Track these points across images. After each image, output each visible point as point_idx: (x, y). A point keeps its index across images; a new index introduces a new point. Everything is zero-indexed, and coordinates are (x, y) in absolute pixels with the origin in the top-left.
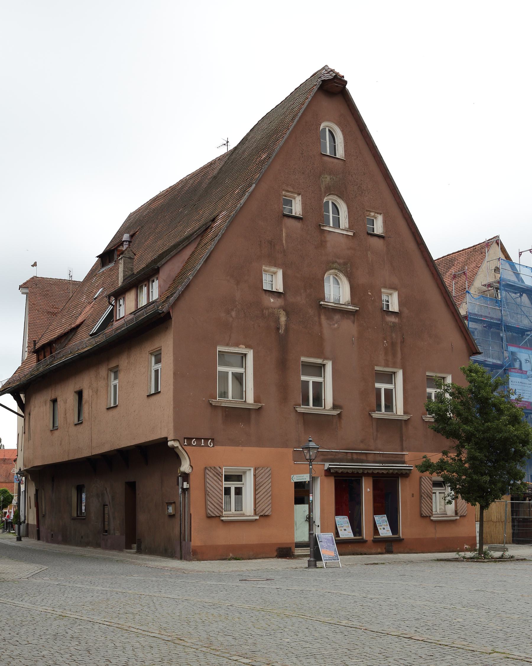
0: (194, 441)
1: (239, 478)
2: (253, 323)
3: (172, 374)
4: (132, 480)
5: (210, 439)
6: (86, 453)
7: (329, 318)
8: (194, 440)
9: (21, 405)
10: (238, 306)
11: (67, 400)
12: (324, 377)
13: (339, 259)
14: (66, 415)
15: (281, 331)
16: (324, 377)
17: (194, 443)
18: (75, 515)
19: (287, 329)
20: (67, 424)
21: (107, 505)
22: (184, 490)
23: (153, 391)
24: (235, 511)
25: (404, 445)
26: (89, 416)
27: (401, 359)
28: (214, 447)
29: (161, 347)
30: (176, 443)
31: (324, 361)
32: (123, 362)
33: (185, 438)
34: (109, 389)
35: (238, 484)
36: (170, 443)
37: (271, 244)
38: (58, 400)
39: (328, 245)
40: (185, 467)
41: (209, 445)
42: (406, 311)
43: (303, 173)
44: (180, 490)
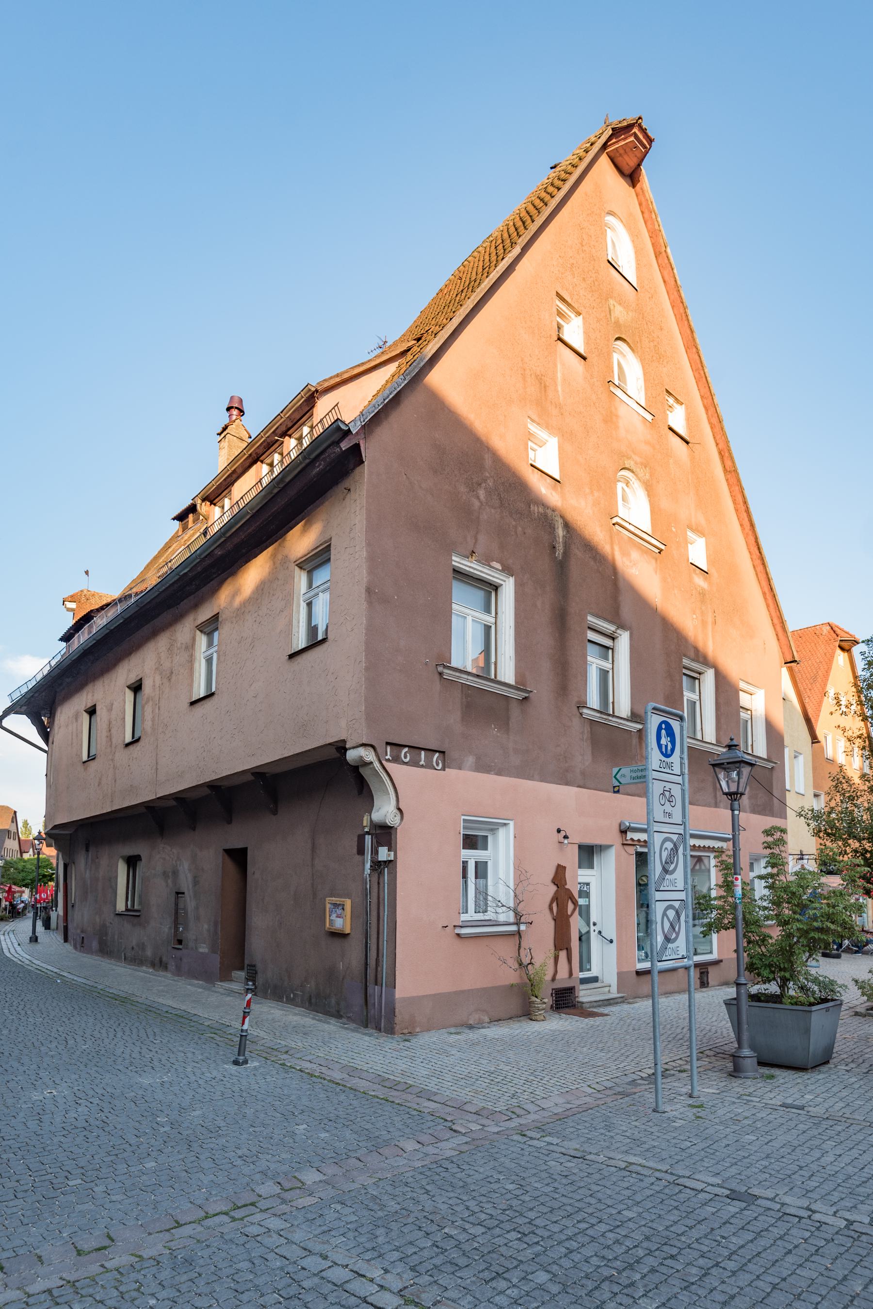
2: (514, 523)
4: (236, 844)
8: (406, 749)
10: (489, 481)
11: (112, 704)
13: (635, 454)
14: (110, 731)
15: (560, 552)
17: (405, 757)
19: (566, 553)
20: (111, 746)
21: (183, 893)
22: (378, 866)
23: (302, 644)
26: (153, 725)
28: (444, 770)
30: (367, 753)
31: (618, 631)
33: (388, 743)
34: (196, 665)
36: (352, 755)
38: (98, 708)
41: (435, 764)
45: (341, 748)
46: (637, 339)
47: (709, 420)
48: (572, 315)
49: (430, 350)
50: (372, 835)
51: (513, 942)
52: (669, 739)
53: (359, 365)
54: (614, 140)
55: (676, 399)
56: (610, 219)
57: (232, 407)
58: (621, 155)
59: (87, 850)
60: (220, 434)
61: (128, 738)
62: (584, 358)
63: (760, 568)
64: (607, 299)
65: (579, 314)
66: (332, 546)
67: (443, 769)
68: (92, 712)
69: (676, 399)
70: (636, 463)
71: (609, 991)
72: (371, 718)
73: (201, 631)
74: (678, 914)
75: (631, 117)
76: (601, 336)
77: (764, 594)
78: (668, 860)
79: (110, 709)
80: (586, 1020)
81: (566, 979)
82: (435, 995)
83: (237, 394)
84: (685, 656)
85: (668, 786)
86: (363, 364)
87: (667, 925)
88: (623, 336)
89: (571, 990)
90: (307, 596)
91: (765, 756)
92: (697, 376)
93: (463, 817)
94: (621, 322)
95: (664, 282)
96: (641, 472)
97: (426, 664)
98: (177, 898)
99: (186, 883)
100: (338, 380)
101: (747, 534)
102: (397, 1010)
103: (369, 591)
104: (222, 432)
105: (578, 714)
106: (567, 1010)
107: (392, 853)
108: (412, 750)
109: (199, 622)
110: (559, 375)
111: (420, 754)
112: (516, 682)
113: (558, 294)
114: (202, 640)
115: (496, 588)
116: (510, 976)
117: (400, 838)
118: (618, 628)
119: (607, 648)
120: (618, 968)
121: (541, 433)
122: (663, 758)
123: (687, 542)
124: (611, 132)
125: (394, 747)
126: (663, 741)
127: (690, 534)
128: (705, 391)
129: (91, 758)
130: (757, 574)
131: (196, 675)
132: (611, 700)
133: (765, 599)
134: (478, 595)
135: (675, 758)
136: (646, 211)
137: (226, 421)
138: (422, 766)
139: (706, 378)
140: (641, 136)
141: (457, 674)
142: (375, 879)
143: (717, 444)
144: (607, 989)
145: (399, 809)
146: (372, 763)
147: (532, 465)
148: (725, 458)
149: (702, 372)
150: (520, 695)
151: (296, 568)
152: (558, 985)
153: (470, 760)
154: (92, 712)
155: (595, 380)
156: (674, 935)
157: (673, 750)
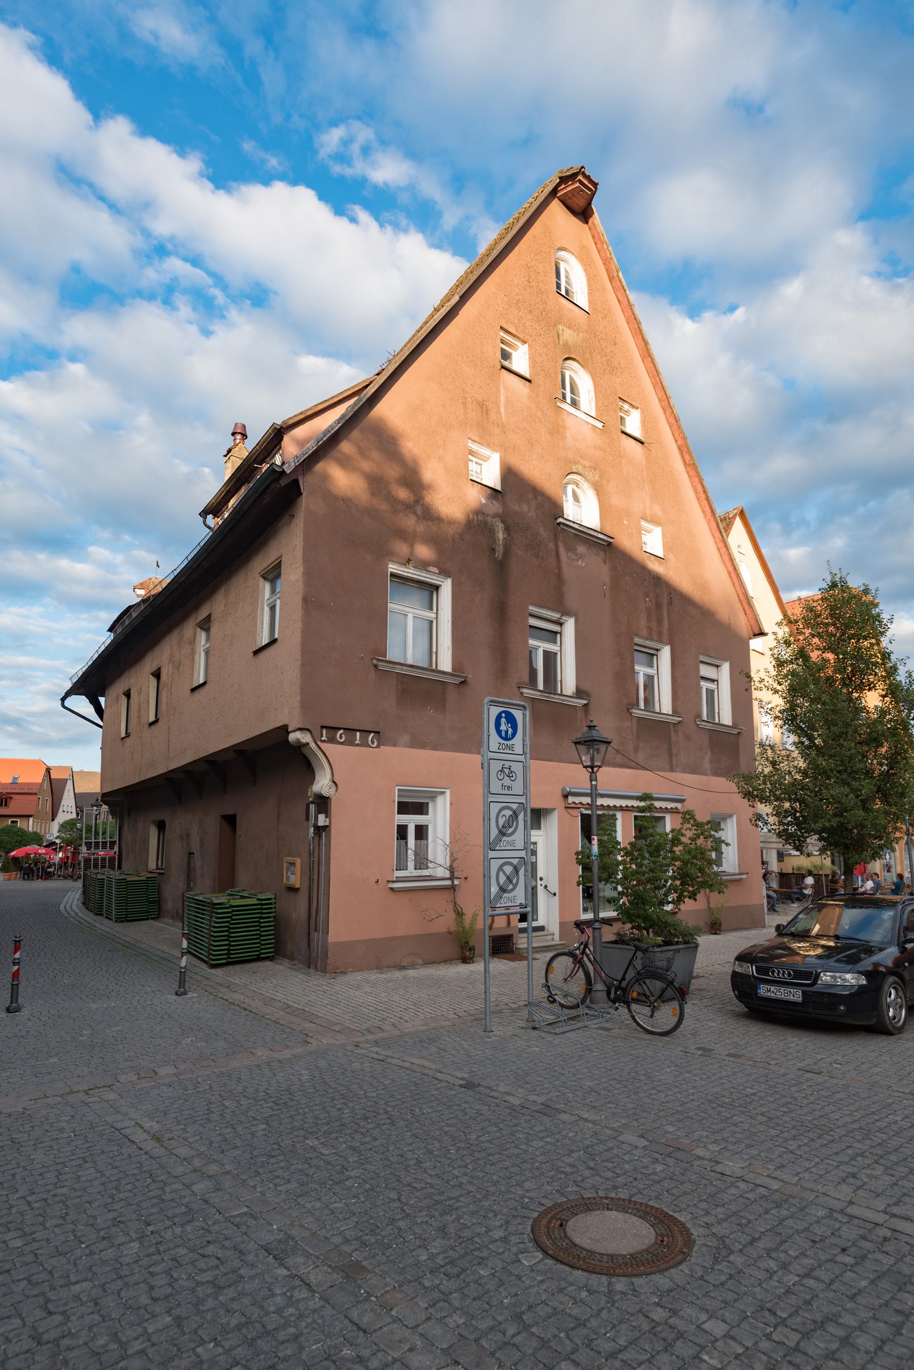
0: (341, 734)
1: (420, 809)
3: (301, 600)
4: (231, 812)
5: (371, 732)
6: (161, 769)
7: (570, 549)
8: (342, 731)
9: (100, 711)
12: (561, 644)
15: (499, 554)
16: (561, 644)
17: (341, 738)
18: (154, 867)
19: (506, 553)
21: (193, 854)
22: (319, 830)
23: (265, 640)
24: (415, 869)
25: (674, 763)
27: (668, 629)
29: (281, 557)
31: (563, 618)
32: (217, 606)
33: (323, 727)
34: (197, 657)
35: (420, 819)
36: (292, 737)
37: (483, 408)
39: (568, 434)
40: (322, 784)
41: (370, 743)
42: (672, 558)
43: (530, 311)
44: (312, 830)
45: (284, 730)
46: (588, 356)
47: (667, 420)
48: (519, 344)
49: (365, 395)
50: (315, 804)
51: (447, 895)
52: (509, 725)
53: (322, 403)
54: (563, 186)
55: (631, 405)
56: (562, 254)
57: (236, 433)
58: (570, 198)
59: (129, 816)
60: (226, 456)
61: (152, 718)
62: (529, 381)
63: (723, 550)
64: (555, 325)
65: (524, 342)
66: (282, 563)
67: (378, 747)
68: (128, 694)
69: (631, 405)
70: (584, 467)
71: (553, 939)
72: (305, 706)
73: (201, 628)
74: (516, 870)
75: (576, 167)
76: (548, 359)
77: (729, 573)
78: (506, 825)
79: (140, 694)
80: (512, 963)
81: (503, 928)
82: (368, 940)
83: (241, 421)
84: (636, 635)
85: (507, 764)
86: (326, 401)
87: (503, 879)
88: (572, 356)
89: (509, 938)
90: (269, 601)
91: (730, 724)
92: (653, 381)
93: (397, 788)
94: (570, 343)
95: (619, 301)
96: (590, 476)
97: (362, 658)
98: (189, 859)
99: (195, 845)
100: (302, 417)
101: (710, 520)
102: (329, 953)
103: (305, 600)
104: (228, 454)
105: (519, 693)
106: (504, 955)
107: (328, 819)
108: (347, 731)
109: (199, 620)
110: (502, 399)
111: (356, 735)
112: (453, 669)
113: (502, 328)
114: (202, 636)
115: (437, 588)
116: (445, 922)
117: (334, 807)
118: (563, 615)
119: (556, 633)
120: (560, 918)
121: (485, 451)
122: (502, 741)
123: (639, 531)
124: (558, 180)
125: (330, 730)
126: (503, 727)
127: (644, 524)
128: (661, 394)
129: (128, 735)
130: (721, 556)
131: (197, 665)
132: (559, 679)
133: (731, 578)
134: (419, 596)
135: (517, 741)
136: (599, 242)
137: (231, 444)
138: (358, 745)
139: (661, 383)
140: (586, 182)
141: (391, 665)
142: (316, 842)
143: (676, 441)
144: (550, 937)
145: (334, 782)
146: (308, 744)
147: (472, 480)
148: (684, 453)
149: (658, 379)
150: (458, 680)
151: (261, 578)
152: (495, 933)
153: (406, 738)
154: (128, 694)
155: (541, 398)
156: (511, 887)
157: (514, 735)
